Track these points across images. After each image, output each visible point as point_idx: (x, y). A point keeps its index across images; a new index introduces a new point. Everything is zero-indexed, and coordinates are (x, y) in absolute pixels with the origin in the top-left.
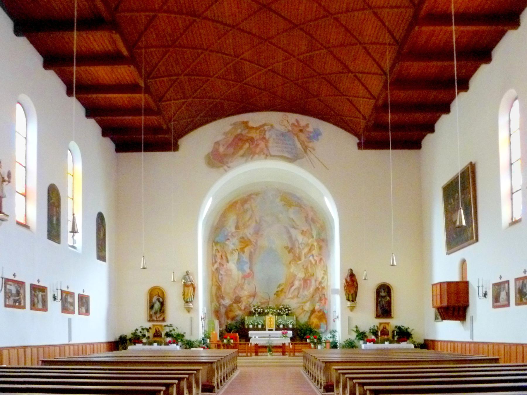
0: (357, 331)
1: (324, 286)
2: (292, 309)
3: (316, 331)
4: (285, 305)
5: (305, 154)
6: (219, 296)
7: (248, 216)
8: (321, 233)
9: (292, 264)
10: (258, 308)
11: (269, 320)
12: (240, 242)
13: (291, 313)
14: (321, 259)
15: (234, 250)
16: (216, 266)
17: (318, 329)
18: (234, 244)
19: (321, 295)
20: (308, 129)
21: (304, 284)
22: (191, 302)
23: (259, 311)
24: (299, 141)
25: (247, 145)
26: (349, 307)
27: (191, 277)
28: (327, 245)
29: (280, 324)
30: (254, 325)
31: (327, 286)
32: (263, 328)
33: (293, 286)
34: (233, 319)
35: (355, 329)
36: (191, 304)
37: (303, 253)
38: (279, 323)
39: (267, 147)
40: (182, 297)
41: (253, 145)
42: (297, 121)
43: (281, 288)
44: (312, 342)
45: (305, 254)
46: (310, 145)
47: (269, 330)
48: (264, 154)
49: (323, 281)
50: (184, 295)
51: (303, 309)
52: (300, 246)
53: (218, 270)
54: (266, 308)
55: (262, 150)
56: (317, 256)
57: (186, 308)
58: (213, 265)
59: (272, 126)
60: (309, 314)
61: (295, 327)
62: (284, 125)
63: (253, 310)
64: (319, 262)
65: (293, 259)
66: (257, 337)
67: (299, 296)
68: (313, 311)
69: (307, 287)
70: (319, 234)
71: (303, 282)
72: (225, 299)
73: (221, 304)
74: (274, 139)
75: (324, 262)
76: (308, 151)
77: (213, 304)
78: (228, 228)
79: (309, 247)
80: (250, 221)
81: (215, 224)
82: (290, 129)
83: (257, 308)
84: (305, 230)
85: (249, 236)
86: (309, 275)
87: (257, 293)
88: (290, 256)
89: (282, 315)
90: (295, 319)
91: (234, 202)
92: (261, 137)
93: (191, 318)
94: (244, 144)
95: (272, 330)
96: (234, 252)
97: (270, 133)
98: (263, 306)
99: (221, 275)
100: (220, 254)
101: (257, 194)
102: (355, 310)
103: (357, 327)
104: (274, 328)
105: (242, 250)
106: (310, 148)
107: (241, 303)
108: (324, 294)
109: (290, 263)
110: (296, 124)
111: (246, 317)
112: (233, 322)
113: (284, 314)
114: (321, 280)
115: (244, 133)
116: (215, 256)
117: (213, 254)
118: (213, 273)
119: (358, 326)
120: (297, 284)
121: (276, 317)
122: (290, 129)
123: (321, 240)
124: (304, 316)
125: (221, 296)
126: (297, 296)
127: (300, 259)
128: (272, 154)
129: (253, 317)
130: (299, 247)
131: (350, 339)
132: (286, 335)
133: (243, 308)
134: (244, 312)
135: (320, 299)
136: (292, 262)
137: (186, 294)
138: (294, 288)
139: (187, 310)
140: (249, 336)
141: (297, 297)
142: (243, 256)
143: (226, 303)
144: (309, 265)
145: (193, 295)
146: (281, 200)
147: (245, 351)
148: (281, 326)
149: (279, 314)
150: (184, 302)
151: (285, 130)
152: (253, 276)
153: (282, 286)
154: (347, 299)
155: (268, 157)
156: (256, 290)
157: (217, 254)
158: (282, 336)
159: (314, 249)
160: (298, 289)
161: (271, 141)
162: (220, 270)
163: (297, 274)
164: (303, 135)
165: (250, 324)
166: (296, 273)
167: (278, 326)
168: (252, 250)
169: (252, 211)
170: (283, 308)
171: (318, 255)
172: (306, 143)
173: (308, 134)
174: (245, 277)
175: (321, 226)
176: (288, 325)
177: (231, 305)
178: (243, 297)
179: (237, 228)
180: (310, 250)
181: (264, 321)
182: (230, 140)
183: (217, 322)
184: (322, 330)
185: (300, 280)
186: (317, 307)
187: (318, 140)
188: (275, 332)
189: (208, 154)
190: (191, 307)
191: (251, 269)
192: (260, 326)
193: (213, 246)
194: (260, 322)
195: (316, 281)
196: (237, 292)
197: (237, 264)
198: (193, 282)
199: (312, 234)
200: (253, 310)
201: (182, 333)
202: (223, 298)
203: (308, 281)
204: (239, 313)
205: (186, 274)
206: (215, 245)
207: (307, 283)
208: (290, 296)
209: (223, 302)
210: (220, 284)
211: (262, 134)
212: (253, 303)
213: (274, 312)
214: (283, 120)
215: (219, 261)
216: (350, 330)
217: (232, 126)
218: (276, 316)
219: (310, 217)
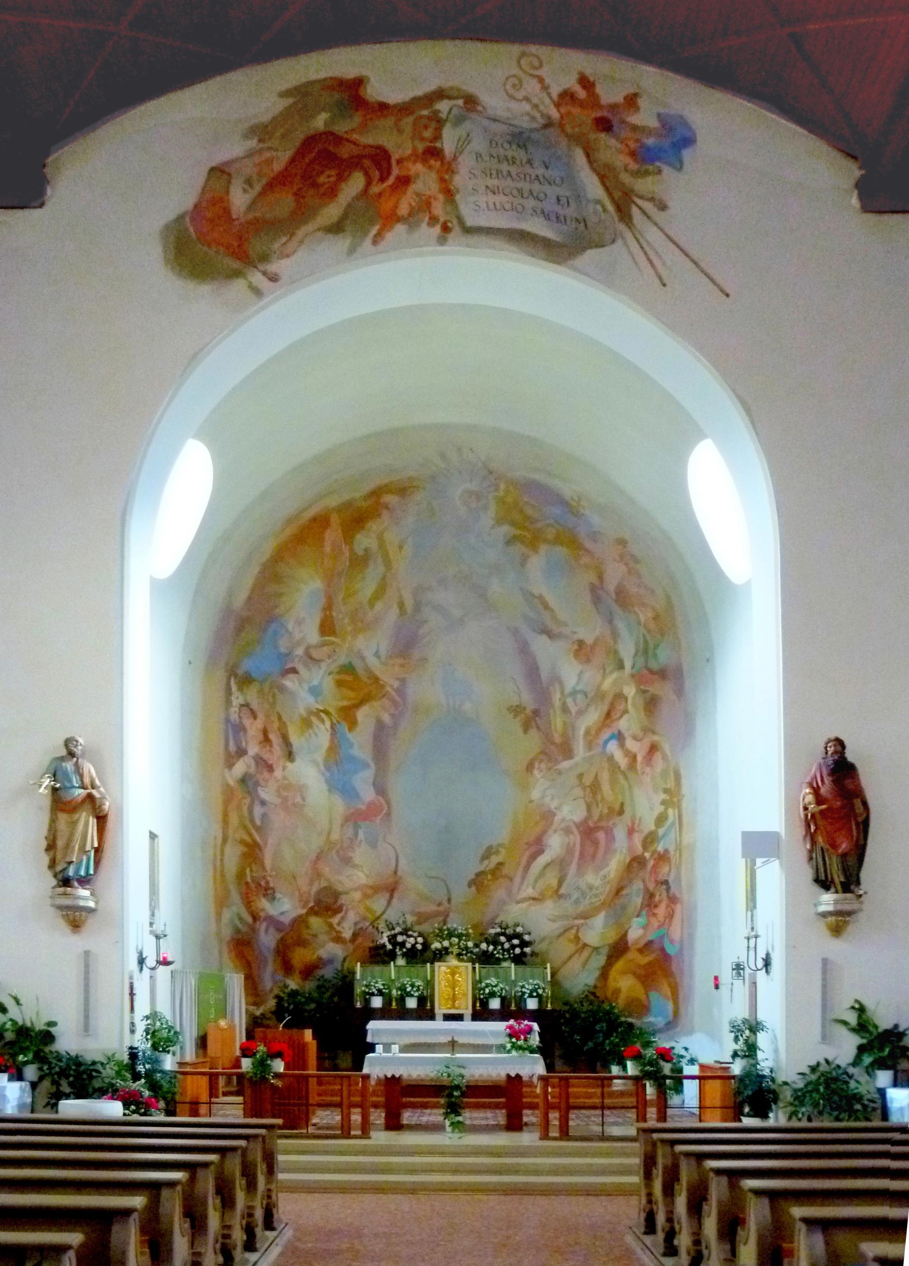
0: (862, 1027)
1: (666, 851)
2: (538, 940)
3: (631, 1026)
4: (511, 924)
5: (622, 227)
6: (253, 885)
7: (367, 586)
8: (656, 647)
9: (536, 772)
10: (405, 932)
11: (448, 981)
12: (340, 684)
13: (533, 954)
14: (653, 748)
15: (317, 713)
16: (240, 767)
17: (640, 1015)
18: (315, 691)
19: (651, 887)
20: (635, 119)
21: (582, 845)
22: (84, 881)
23: (408, 946)
24: (594, 170)
25: (356, 183)
26: (824, 915)
27: (89, 769)
28: (680, 692)
29: (492, 995)
30: (388, 1000)
31: (679, 848)
32: (425, 1012)
33: (541, 852)
34: (308, 972)
35: (852, 1018)
36: (84, 892)
37: (582, 732)
38: (487, 991)
39: (449, 193)
40: (46, 859)
41: (382, 179)
42: (585, 82)
43: (495, 860)
44: (646, 1075)
45: (588, 732)
46: (644, 185)
47: (448, 1017)
48: (433, 220)
49: (661, 831)
50: (51, 847)
51: (577, 938)
52: (569, 701)
53: (250, 784)
54: (438, 936)
55: (426, 204)
56: (635, 738)
57: (60, 908)
58: (230, 765)
59: (471, 102)
60: (600, 960)
61: (549, 1007)
62: (527, 99)
63: (385, 940)
64: (645, 757)
65: (543, 752)
66: (395, 1048)
67: (562, 891)
68: (619, 949)
69: (594, 857)
70: (645, 651)
71: (578, 838)
72: (278, 895)
73: (262, 914)
74: (479, 156)
75: (665, 758)
76: (635, 210)
77: (227, 915)
78: (290, 626)
79: (605, 708)
80: (379, 606)
81: (240, 600)
82: (555, 114)
83: (401, 934)
84: (589, 641)
85: (372, 662)
86: (606, 811)
87: (401, 878)
88: (531, 743)
89: (498, 961)
90: (549, 979)
91: (314, 520)
92: (421, 147)
93: (87, 953)
94: (341, 178)
95: (459, 1018)
96: (314, 719)
97: (461, 131)
98: (426, 928)
99: (263, 803)
100: (259, 724)
101: (403, 490)
102: (854, 929)
103: (861, 1010)
104: (468, 1012)
105: (348, 715)
106: (641, 197)
107: (339, 916)
108: (666, 882)
109: (530, 767)
110: (582, 94)
111: (359, 964)
112: (310, 986)
113: (505, 960)
114: (653, 828)
115: (342, 128)
116: (239, 729)
117: (227, 720)
118: (228, 795)
119: (869, 1003)
120: (555, 844)
121: (474, 968)
122: (555, 114)
123: (651, 672)
124: (584, 965)
125: (263, 883)
126: (557, 891)
127: (567, 751)
128: (471, 221)
129: (385, 968)
130: (565, 709)
131: (827, 1061)
132: (526, 1040)
133: (347, 934)
134: (351, 947)
135: (650, 902)
136: (536, 765)
137: (60, 843)
138: (542, 860)
139: (66, 917)
140: (369, 1039)
141: (558, 895)
142: (350, 736)
143: (282, 913)
144: (605, 777)
145: (98, 851)
146: (499, 522)
147: (337, 1099)
148: (495, 1004)
149: (486, 959)
150: (54, 882)
151: (533, 118)
152: (388, 814)
153: (497, 852)
154: (817, 880)
155: (451, 236)
156: (400, 869)
157: (247, 722)
158: (509, 1046)
159: (626, 712)
160: (561, 864)
161: (466, 163)
162: (257, 784)
163: (558, 808)
164: (613, 142)
165: (373, 994)
166: (553, 805)
167: (484, 1003)
168: (386, 718)
169: (388, 563)
170: (503, 934)
171: (641, 734)
172: (626, 178)
173: (637, 141)
174: (355, 818)
175: (656, 618)
176: (521, 1000)
177: (299, 922)
178: (347, 893)
179: (327, 627)
180: (608, 715)
181: (430, 984)
182: (282, 158)
183: (236, 982)
184: (655, 1019)
185: (567, 831)
186: (635, 934)
187: (679, 166)
188: (468, 1025)
189: (180, 218)
190: (82, 903)
191: (381, 789)
192: (412, 1003)
193: (228, 692)
194: (412, 986)
195: (631, 831)
196: (326, 870)
197: (328, 768)
198: (94, 792)
199: (616, 652)
200: (385, 940)
201: (40, 1026)
202: (268, 892)
203: (601, 835)
204: (330, 950)
205: (64, 752)
206: (240, 689)
207: (596, 843)
208: (529, 891)
209: (264, 905)
210: (258, 839)
211: (428, 134)
212: (385, 917)
213: (467, 948)
214: (523, 76)
215: (253, 749)
216: (830, 1021)
217: (290, 101)
218: (477, 966)
219: (611, 584)
